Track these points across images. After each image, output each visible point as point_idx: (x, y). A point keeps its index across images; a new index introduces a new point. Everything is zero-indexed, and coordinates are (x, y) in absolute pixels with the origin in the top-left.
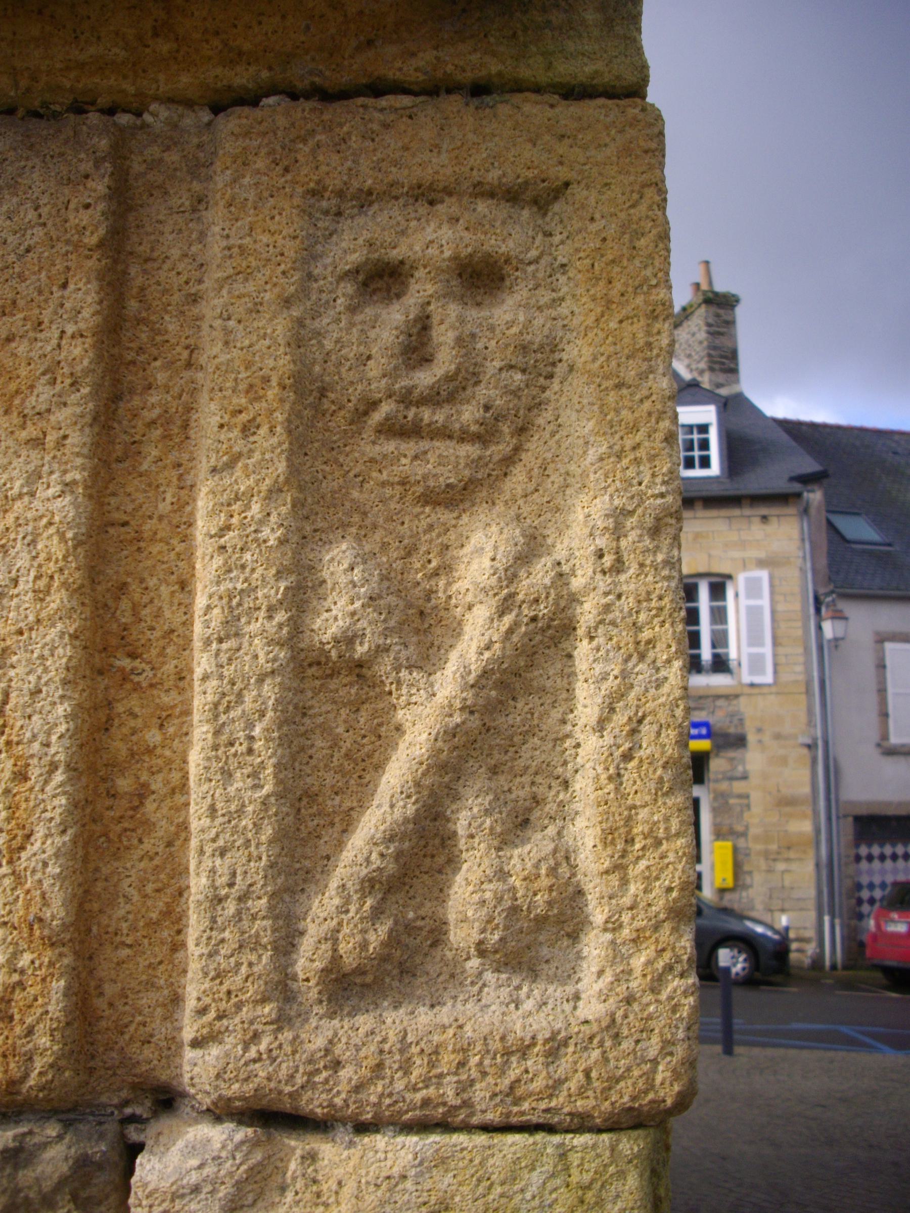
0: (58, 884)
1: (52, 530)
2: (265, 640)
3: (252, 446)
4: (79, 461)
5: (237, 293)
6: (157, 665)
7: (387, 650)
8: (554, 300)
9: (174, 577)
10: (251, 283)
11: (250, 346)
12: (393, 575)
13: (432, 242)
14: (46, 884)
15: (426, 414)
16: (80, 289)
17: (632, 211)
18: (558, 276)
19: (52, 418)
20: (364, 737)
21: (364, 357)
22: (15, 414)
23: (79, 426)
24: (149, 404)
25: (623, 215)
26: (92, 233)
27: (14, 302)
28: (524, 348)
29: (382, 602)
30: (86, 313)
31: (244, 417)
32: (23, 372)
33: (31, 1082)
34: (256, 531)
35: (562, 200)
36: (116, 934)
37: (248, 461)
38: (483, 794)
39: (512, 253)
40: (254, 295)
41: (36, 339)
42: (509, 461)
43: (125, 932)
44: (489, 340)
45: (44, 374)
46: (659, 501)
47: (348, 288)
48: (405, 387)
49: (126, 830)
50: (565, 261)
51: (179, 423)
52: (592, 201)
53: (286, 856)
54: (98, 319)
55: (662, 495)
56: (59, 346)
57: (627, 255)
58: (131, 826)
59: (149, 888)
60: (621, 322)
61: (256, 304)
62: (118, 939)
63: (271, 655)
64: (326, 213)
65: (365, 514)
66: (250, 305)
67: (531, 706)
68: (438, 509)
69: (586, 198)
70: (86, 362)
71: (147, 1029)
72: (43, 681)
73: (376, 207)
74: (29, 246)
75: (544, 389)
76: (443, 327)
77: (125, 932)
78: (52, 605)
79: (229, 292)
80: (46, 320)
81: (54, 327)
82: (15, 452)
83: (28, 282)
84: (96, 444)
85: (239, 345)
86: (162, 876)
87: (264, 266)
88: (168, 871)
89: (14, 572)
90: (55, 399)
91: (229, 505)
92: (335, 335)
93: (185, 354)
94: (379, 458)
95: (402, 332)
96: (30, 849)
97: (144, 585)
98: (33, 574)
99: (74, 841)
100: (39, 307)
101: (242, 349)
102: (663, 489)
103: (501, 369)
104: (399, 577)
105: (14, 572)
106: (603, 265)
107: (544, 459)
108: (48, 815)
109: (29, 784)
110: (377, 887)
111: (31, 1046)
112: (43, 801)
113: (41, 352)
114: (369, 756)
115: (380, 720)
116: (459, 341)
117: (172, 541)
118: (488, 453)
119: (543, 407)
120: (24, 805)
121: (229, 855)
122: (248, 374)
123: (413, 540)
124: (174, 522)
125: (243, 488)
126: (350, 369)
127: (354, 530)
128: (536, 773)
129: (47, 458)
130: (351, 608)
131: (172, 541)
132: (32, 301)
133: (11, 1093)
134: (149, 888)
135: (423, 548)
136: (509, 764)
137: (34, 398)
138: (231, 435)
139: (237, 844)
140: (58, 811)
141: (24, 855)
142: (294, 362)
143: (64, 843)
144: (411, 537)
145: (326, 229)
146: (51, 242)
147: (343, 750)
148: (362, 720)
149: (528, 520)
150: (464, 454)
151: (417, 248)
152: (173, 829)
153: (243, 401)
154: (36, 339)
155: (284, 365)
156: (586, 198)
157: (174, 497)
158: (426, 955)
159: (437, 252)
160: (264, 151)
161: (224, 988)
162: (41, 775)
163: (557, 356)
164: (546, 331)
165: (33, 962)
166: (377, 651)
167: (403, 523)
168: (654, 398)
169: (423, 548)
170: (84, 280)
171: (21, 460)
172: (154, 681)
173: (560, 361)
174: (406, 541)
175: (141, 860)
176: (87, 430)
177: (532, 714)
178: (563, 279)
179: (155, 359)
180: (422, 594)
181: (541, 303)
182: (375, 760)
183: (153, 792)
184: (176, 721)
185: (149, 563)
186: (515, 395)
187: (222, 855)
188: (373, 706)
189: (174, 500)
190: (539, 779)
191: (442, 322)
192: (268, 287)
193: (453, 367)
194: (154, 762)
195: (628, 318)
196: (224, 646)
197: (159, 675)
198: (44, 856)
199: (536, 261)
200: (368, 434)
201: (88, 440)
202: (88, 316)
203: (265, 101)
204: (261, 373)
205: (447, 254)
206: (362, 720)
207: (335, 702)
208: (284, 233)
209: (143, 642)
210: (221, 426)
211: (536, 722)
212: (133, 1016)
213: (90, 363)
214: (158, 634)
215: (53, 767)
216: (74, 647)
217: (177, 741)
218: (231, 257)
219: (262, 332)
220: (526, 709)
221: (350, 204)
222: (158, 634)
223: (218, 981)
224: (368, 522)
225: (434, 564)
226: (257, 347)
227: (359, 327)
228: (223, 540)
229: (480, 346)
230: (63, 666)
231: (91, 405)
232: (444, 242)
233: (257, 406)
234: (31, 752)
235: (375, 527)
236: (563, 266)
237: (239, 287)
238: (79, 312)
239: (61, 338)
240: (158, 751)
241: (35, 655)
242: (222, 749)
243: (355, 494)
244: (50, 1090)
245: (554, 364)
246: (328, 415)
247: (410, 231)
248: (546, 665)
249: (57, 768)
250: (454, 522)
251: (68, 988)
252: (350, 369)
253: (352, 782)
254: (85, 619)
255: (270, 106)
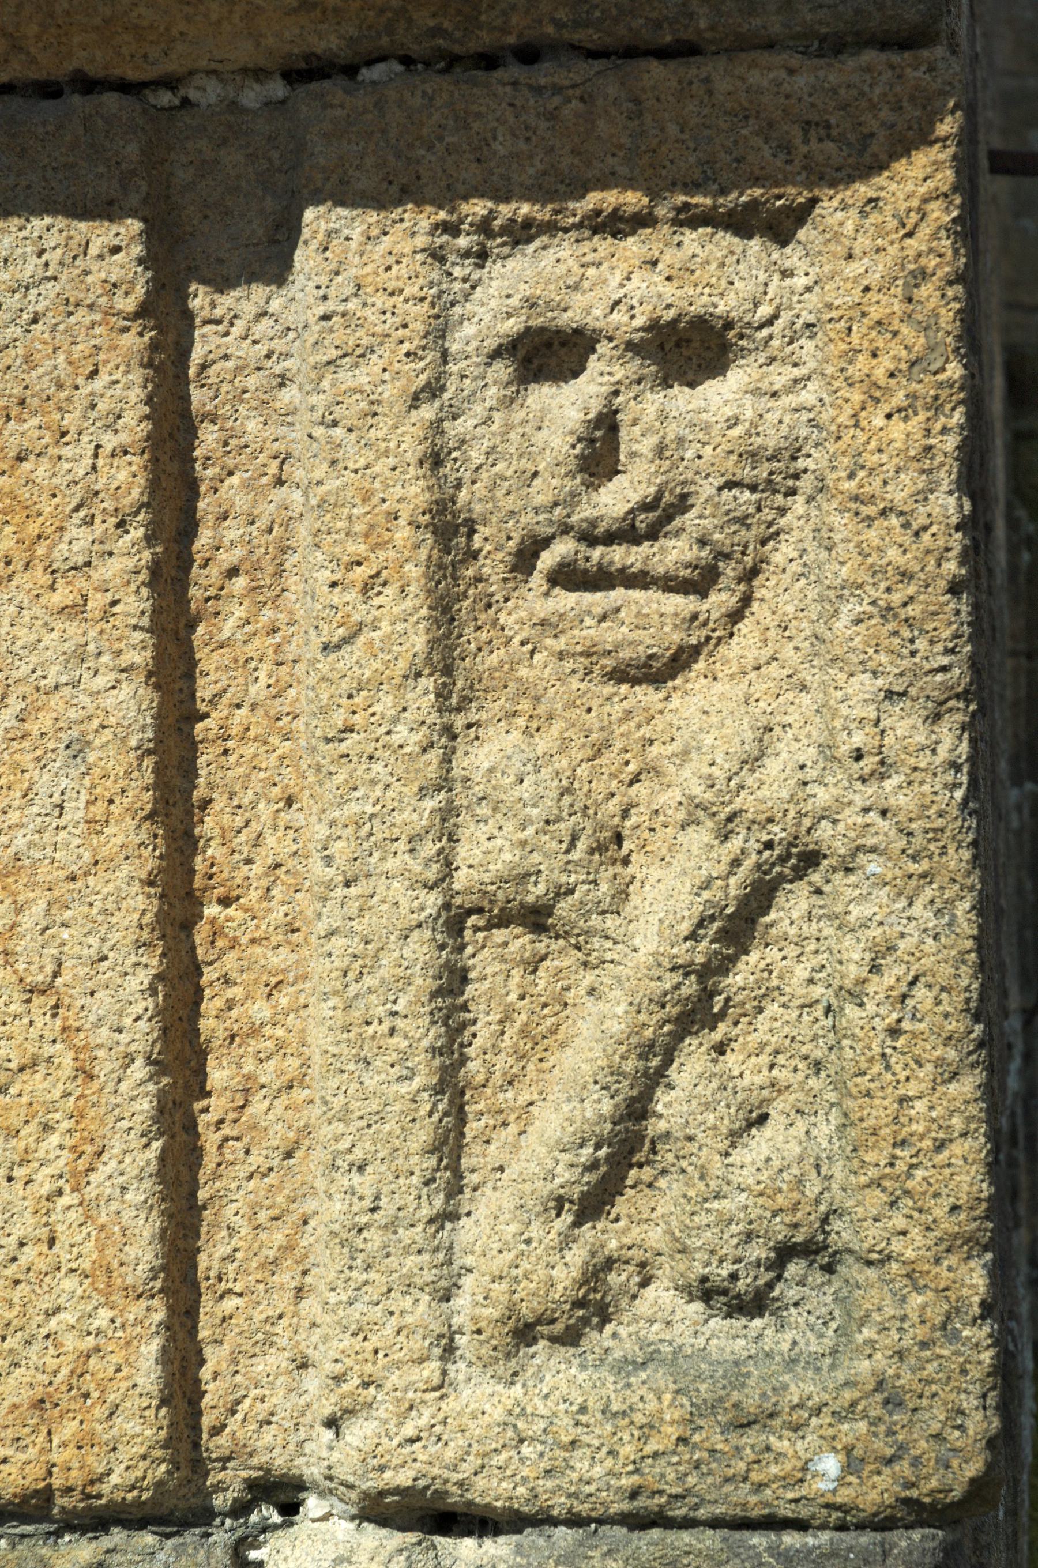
0: (143, 1216)
1: (107, 735)
2: (407, 883)
3: (377, 613)
4: (138, 636)
5: (343, 387)
6: (260, 914)
7: (571, 892)
8: (796, 381)
9: (276, 790)
10: (363, 369)
11: (367, 467)
12: (576, 785)
13: (617, 303)
14: (127, 1214)
15: (619, 555)
16: (117, 382)
17: (908, 241)
18: (803, 341)
19: (95, 576)
20: (545, 1005)
21: (528, 475)
22: (40, 569)
23: (133, 587)
24: (226, 541)
25: (893, 250)
26: (127, 293)
27: (22, 402)
28: (753, 456)
29: (562, 826)
30: (129, 418)
31: (361, 573)
32: (47, 507)
33: (114, 1479)
34: (388, 733)
35: (808, 226)
36: (220, 1280)
37: (373, 634)
38: (704, 1082)
39: (733, 314)
40: (368, 388)
41: (60, 458)
42: (736, 616)
43: (231, 1276)
44: (704, 444)
45: (76, 509)
46: (939, 677)
47: (502, 370)
48: (586, 520)
49: (227, 1139)
50: (811, 319)
51: (271, 569)
52: (850, 226)
53: (446, 1168)
54: (146, 427)
55: (944, 669)
56: (94, 468)
57: (899, 313)
58: (235, 1133)
59: (263, 1216)
60: (889, 416)
61: (372, 403)
62: (223, 1286)
63: (416, 903)
64: (467, 254)
65: (537, 699)
66: (363, 405)
67: (768, 960)
68: (637, 688)
69: (841, 224)
70: (135, 493)
71: (266, 1405)
72: (108, 944)
73: (537, 243)
74: (36, 313)
75: (782, 511)
76: (637, 429)
77: (231, 1276)
78: (114, 840)
79: (333, 385)
80: (73, 429)
81: (85, 438)
82: (46, 624)
83: (41, 370)
84: (156, 612)
85: (351, 466)
86: (280, 1199)
87: (381, 344)
88: (286, 1192)
89: (56, 795)
90: (96, 547)
91: (350, 697)
92: (486, 443)
93: (273, 468)
94: (554, 619)
95: (580, 440)
96: (103, 1171)
97: (235, 803)
98: (84, 797)
99: (162, 1159)
100: (60, 409)
101: (356, 471)
102: (945, 661)
103: (720, 489)
104: (585, 789)
105: (56, 795)
106: (864, 330)
107: (785, 614)
108: (125, 1124)
109: (96, 1085)
110: (567, 1206)
111: (115, 1431)
112: (118, 1105)
113: (69, 478)
114: (554, 1031)
115: (566, 983)
116: (660, 451)
117: (271, 739)
118: (705, 607)
119: (782, 537)
120: (92, 1113)
121: (369, 1169)
122: (367, 509)
123: (605, 734)
124: (272, 713)
125: (368, 673)
126: (508, 493)
127: (521, 721)
128: (777, 1052)
129: (93, 633)
130: (522, 836)
131: (271, 739)
132: (48, 399)
133: (89, 1497)
134: (263, 1216)
135: (618, 745)
136: (741, 1040)
137: (64, 546)
138: (347, 598)
139: (380, 1155)
140: (138, 1118)
141: (93, 1177)
142: (430, 488)
143: (148, 1162)
144: (602, 729)
145: (465, 280)
146: (69, 306)
147: (518, 1025)
148: (542, 984)
149: (761, 704)
150: (672, 610)
151: (597, 312)
152: (291, 1135)
153: (362, 548)
154: (60, 458)
155: (416, 495)
156: (841, 224)
157: (270, 676)
158: (634, 1297)
159: (626, 318)
160: (369, 161)
161: (369, 1346)
162: (113, 1071)
163: (801, 463)
164: (784, 430)
165: (113, 1321)
166: (558, 894)
167: (589, 710)
168: (934, 529)
169: (618, 745)
170: (122, 368)
171: (54, 635)
172: (257, 935)
173: (805, 471)
174: (594, 736)
175: (251, 1177)
176: (145, 592)
177: (771, 972)
178: (809, 345)
179: (231, 473)
180: (618, 810)
181: (776, 387)
182: (560, 1037)
183: (263, 1087)
184: (291, 990)
185: (241, 771)
186: (743, 524)
187: (361, 1169)
188: (556, 963)
189: (271, 681)
190: (781, 1059)
191: (635, 422)
192: (387, 376)
193: (652, 490)
194: (261, 1046)
195: (899, 411)
196: (353, 891)
197: (264, 927)
198: (121, 1179)
199: (770, 322)
200: (537, 580)
201: (147, 605)
202: (134, 423)
203: (366, 74)
204: (385, 506)
205: (639, 322)
206: (542, 984)
207: (505, 961)
208: (406, 293)
209: (238, 881)
210: (334, 585)
211: (775, 982)
212: (247, 1388)
213: (142, 494)
214: (257, 869)
215: (129, 1059)
216: (149, 896)
217: (292, 1016)
218: (331, 330)
219: (383, 445)
220: (762, 965)
221: (499, 240)
222: (257, 869)
223: (361, 1337)
224: (541, 710)
225: (632, 767)
226: (377, 469)
227: (520, 430)
228: (344, 745)
229: (689, 454)
230: (135, 924)
231: (147, 555)
232: (635, 302)
233: (381, 554)
234: (99, 1041)
235: (551, 717)
236: (809, 326)
237: (347, 378)
238: (119, 417)
239: (96, 456)
240: (268, 1030)
241: (95, 911)
242: (355, 1030)
243: (523, 672)
244: (142, 1489)
245: (796, 476)
246: (481, 557)
247: (586, 284)
248: (787, 906)
249: (133, 1060)
250: (660, 706)
251: (164, 1350)
252: (508, 493)
253: (531, 1067)
254: (161, 857)
255: (374, 83)
